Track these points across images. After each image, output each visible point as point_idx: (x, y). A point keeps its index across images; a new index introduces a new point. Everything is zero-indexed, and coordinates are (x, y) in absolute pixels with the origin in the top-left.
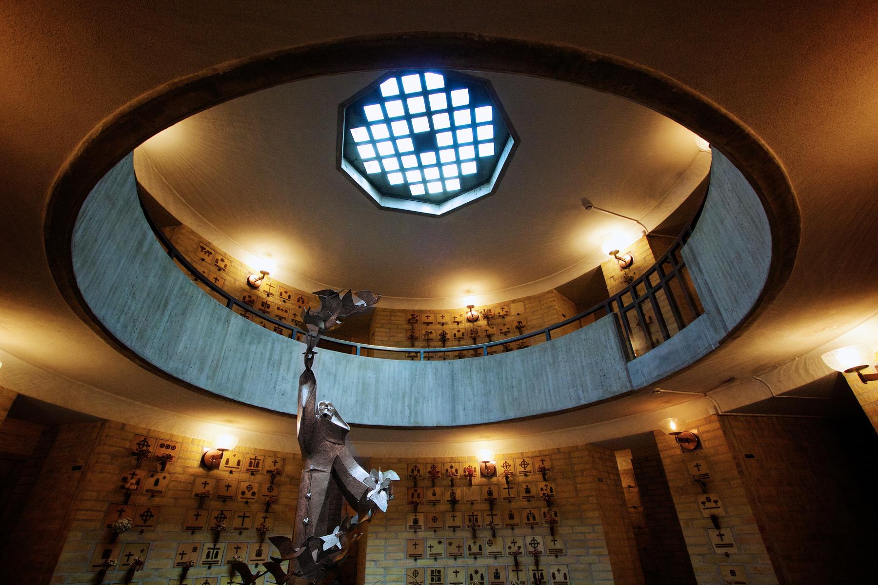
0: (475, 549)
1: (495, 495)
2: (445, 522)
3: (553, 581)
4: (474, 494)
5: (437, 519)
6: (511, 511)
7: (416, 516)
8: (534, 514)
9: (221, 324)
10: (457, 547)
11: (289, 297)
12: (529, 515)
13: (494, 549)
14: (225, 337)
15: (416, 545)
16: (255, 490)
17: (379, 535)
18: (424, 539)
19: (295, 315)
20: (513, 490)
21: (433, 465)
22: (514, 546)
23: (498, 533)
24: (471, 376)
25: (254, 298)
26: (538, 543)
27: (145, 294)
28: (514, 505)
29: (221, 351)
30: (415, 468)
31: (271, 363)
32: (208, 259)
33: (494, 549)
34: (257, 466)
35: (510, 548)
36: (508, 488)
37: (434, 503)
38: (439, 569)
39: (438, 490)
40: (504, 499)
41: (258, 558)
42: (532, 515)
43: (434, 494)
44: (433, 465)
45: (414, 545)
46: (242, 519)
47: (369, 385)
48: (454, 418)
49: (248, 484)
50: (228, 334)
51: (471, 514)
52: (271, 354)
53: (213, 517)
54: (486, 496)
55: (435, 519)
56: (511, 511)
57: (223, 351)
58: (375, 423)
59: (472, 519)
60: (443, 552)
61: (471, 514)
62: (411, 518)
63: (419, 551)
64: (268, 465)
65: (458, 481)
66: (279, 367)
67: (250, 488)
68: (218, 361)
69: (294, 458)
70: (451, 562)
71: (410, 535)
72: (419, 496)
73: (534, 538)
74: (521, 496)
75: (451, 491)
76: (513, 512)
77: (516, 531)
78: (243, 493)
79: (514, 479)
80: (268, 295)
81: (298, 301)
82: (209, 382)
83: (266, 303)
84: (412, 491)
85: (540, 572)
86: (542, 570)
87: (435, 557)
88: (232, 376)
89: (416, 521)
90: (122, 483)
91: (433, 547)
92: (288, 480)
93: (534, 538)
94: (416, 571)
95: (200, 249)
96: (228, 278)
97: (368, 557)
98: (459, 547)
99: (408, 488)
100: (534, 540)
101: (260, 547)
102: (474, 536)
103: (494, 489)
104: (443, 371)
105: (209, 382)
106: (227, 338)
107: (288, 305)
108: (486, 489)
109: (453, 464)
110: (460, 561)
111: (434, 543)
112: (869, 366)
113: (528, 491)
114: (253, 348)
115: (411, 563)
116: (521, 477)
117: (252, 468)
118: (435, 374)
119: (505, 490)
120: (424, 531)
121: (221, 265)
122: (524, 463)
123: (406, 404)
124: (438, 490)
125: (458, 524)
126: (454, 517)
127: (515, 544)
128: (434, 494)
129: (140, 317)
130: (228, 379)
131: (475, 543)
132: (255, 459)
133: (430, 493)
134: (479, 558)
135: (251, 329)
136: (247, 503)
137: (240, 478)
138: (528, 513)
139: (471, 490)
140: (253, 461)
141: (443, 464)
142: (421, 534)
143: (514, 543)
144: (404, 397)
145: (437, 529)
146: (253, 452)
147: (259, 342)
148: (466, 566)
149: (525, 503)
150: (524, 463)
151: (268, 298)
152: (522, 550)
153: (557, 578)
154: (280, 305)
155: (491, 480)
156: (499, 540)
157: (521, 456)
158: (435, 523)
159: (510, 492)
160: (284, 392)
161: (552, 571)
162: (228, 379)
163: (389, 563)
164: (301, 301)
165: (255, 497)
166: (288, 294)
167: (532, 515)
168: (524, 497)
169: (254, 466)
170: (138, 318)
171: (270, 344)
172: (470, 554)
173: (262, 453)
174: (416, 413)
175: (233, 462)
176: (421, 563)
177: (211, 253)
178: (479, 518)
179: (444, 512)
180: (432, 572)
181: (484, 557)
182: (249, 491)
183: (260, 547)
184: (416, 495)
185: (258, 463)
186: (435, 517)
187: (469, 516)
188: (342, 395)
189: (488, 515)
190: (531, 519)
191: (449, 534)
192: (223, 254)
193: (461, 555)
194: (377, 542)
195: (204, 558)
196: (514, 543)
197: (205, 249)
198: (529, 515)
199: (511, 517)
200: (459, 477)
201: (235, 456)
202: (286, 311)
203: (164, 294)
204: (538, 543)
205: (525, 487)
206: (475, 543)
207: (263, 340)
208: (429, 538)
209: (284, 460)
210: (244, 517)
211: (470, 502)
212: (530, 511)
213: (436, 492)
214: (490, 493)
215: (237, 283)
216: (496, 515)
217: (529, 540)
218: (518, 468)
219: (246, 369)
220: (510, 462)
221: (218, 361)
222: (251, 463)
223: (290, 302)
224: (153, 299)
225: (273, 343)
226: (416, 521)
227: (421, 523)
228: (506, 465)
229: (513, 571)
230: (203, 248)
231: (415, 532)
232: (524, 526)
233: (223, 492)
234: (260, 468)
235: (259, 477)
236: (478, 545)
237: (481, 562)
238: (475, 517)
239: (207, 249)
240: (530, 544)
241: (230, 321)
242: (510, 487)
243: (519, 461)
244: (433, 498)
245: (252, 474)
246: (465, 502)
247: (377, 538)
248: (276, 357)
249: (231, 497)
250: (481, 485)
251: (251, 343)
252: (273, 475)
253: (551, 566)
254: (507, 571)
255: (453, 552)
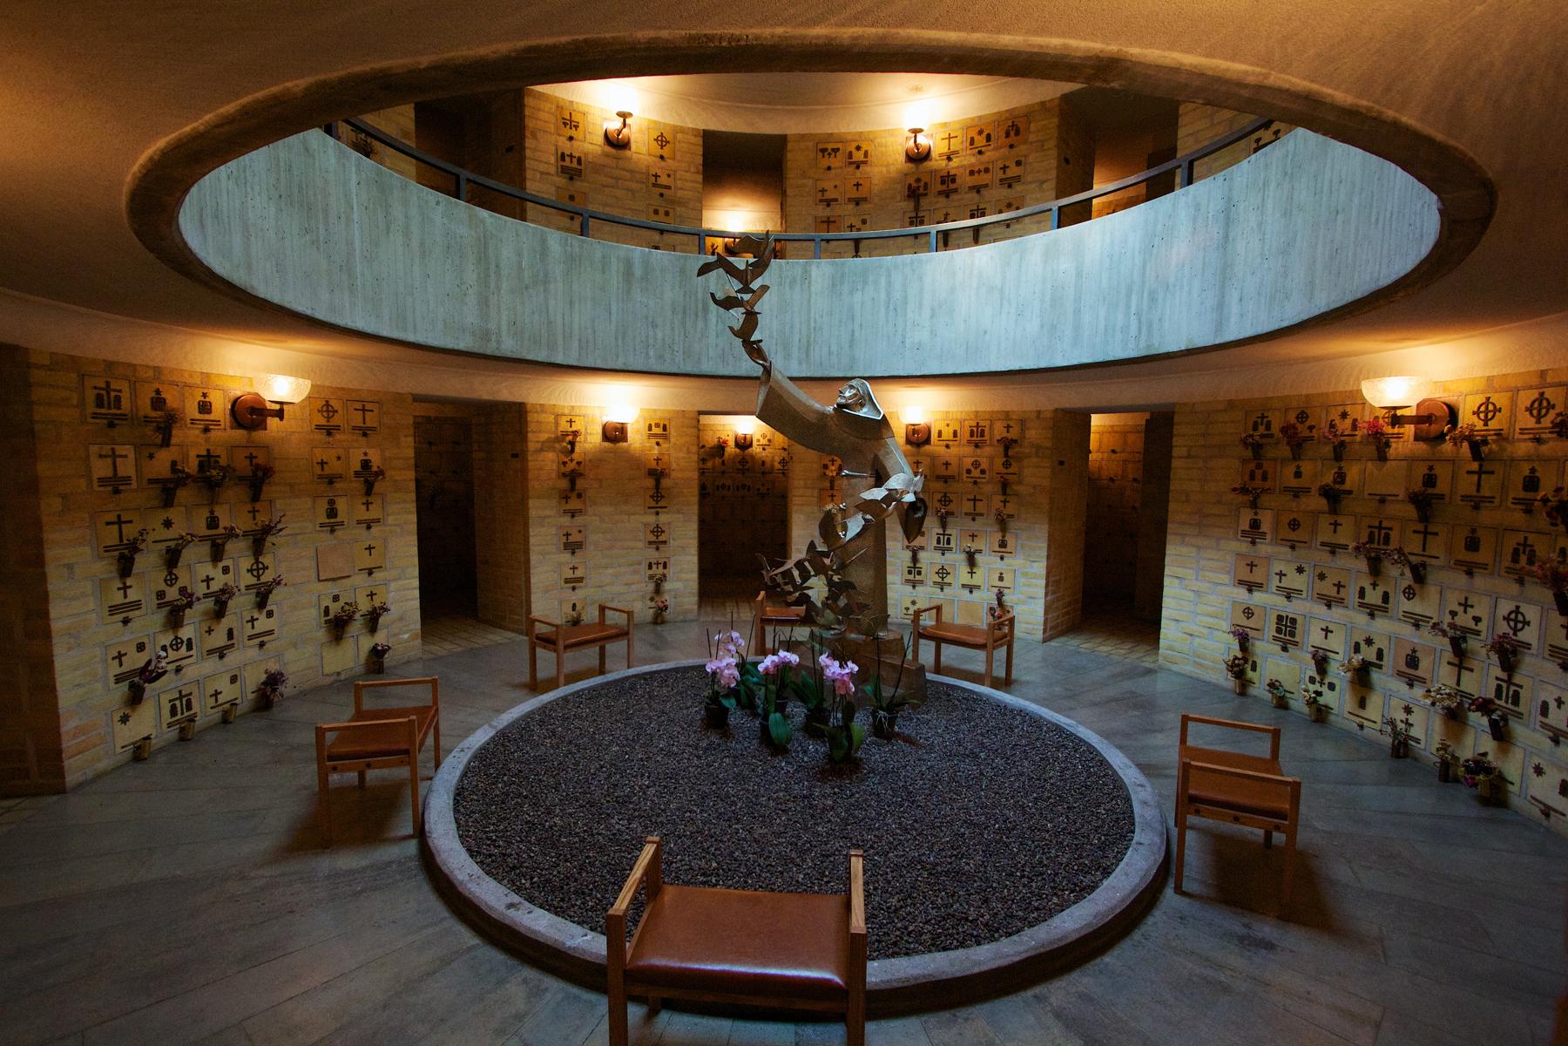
0: (1373, 597)
1: (1442, 486)
2: (1316, 534)
3: (1540, 718)
4: (1393, 480)
5: (1299, 525)
6: (1474, 531)
7: (1256, 514)
8: (1536, 548)
9: (798, 288)
10: (1335, 585)
11: (988, 138)
12: (1521, 548)
13: (1416, 606)
14: (809, 301)
15: (1252, 565)
16: (984, 466)
17: (1187, 539)
18: (1268, 558)
19: (1004, 168)
20: (1492, 477)
21: (1303, 412)
22: (1465, 612)
23: (1433, 577)
24: (1263, 206)
25: (925, 179)
26: (1526, 623)
27: (669, 314)
28: (1486, 516)
29: (809, 321)
30: (1263, 420)
31: (891, 308)
32: (835, 162)
33: (1416, 606)
34: (982, 436)
35: (1453, 614)
36: (1480, 473)
37: (1297, 493)
38: (1294, 616)
39: (1307, 467)
40: (1464, 498)
41: (1003, 550)
42: (1528, 549)
43: (1298, 475)
44: (1303, 412)
45: (1248, 565)
46: (972, 503)
47: (1063, 288)
48: (1219, 326)
49: (973, 459)
50: (813, 296)
51: (1377, 524)
52: (888, 294)
53: (935, 500)
54: (1417, 486)
55: (1294, 525)
56: (1474, 531)
57: (812, 321)
58: (1075, 362)
59: (1376, 534)
60: (1303, 588)
61: (1377, 524)
62: (1245, 518)
63: (1257, 577)
64: (999, 431)
65: (1357, 446)
66: (906, 308)
67: (976, 464)
68: (809, 336)
69: (1038, 417)
70: (1320, 609)
71: (1243, 546)
72: (1265, 478)
73: (1518, 607)
74: (1511, 495)
75: (1336, 470)
76: (1480, 533)
77: (1480, 581)
78: (969, 471)
79: (1503, 450)
80: (949, 159)
81: (1008, 135)
82: (804, 365)
83: (948, 176)
84: (1252, 466)
85: (1512, 688)
86: (1521, 687)
87: (1289, 595)
88: (834, 348)
89: (1255, 525)
90: (823, 470)
91: (1285, 575)
92: (1034, 449)
93: (1518, 607)
94: (1249, 608)
95: (820, 154)
96: (876, 170)
97: (1167, 571)
98: (1339, 586)
99: (1244, 461)
100: (1517, 611)
101: (1004, 537)
102: (1375, 570)
103: (1442, 472)
104: (1211, 205)
105: (804, 365)
106: (812, 301)
107: (990, 155)
108: (1421, 470)
109: (1348, 409)
110: (1337, 613)
111: (1290, 570)
112: (698, 275)
113: (1531, 483)
114: (858, 297)
115: (1241, 594)
116: (1523, 445)
117: (974, 438)
118: (1195, 220)
119: (1470, 476)
120: (1270, 544)
121: (859, 156)
122: (1487, 408)
123: (1133, 310)
124: (1307, 467)
125: (1342, 541)
126: (1336, 524)
127: (1469, 609)
128: (1298, 475)
129: (676, 337)
130: (830, 353)
131: (1374, 585)
132: (978, 426)
133: (1290, 470)
134: (1381, 617)
135: (847, 270)
136: (975, 483)
137: (961, 453)
138: (1518, 544)
139: (1384, 470)
140: (975, 429)
141: (1327, 408)
142: (1264, 548)
143: (1466, 605)
144: (1129, 296)
145: (1297, 544)
146: (973, 417)
147: (865, 283)
148: (1349, 625)
149: (1517, 517)
150: (1487, 408)
151: (951, 163)
152: (1482, 626)
153: (1550, 715)
154: (972, 165)
155: (1439, 448)
156: (1432, 591)
157: (1535, 381)
158: (1294, 533)
159: (1482, 483)
160: (920, 344)
161: (1543, 696)
162: (830, 353)
163: (1204, 586)
164: (1012, 133)
165: (987, 476)
166: (985, 134)
167: (1528, 549)
168: (1517, 501)
169: (977, 435)
170: (673, 340)
171: (883, 281)
172: (1361, 605)
173: (987, 417)
174: (1150, 326)
175: (947, 434)
176: (1258, 597)
177: (838, 149)
178: (1394, 535)
179: (1315, 514)
180: (1280, 618)
181: (1391, 618)
182: (976, 468)
183: (1004, 537)
184: (1259, 473)
185: (983, 431)
186: (1295, 520)
187: (1369, 527)
188: (1016, 321)
189: (1415, 532)
190: (1523, 559)
191: (1323, 557)
192: (856, 137)
193: (1341, 602)
194: (1185, 550)
195: (935, 543)
196: (1466, 605)
197: (826, 150)
198: (1521, 548)
199: (1473, 544)
200: (1358, 439)
201: (948, 425)
202: (987, 170)
203: (697, 299)
204: (1526, 623)
205: (1527, 473)
206: (1374, 585)
207: (871, 278)
208: (1279, 560)
209: (1023, 422)
210: (975, 500)
211: (1378, 497)
212: (1526, 538)
213: (1302, 469)
214: (1430, 480)
215: (892, 169)
216: (1436, 534)
217: (1505, 607)
218: (1520, 417)
219: (853, 331)
220: (1500, 400)
221: (809, 336)
222: (972, 431)
223: (992, 147)
224: (684, 313)
225: (889, 276)
226: (1255, 525)
227: (1265, 527)
228: (1487, 410)
229: (1449, 663)
230: (824, 150)
231: (1253, 543)
232: (1502, 573)
233: (942, 471)
234: (987, 437)
235: (987, 450)
236: (1380, 590)
237: (1382, 627)
238: (1383, 532)
239: (830, 146)
240: (1507, 619)
241: (810, 276)
242: (1484, 469)
243: (1526, 398)
244: (1294, 483)
245: (977, 446)
246: (1367, 497)
247: (1183, 542)
248: (897, 295)
249: (953, 477)
250: (1411, 460)
251: (851, 293)
252: (1007, 444)
253: (1546, 685)
254: (1437, 659)
255: (1325, 592)
